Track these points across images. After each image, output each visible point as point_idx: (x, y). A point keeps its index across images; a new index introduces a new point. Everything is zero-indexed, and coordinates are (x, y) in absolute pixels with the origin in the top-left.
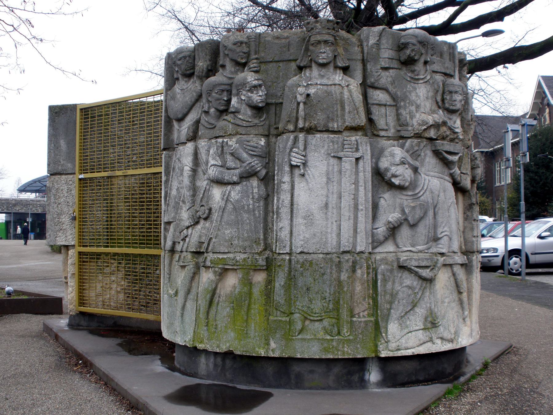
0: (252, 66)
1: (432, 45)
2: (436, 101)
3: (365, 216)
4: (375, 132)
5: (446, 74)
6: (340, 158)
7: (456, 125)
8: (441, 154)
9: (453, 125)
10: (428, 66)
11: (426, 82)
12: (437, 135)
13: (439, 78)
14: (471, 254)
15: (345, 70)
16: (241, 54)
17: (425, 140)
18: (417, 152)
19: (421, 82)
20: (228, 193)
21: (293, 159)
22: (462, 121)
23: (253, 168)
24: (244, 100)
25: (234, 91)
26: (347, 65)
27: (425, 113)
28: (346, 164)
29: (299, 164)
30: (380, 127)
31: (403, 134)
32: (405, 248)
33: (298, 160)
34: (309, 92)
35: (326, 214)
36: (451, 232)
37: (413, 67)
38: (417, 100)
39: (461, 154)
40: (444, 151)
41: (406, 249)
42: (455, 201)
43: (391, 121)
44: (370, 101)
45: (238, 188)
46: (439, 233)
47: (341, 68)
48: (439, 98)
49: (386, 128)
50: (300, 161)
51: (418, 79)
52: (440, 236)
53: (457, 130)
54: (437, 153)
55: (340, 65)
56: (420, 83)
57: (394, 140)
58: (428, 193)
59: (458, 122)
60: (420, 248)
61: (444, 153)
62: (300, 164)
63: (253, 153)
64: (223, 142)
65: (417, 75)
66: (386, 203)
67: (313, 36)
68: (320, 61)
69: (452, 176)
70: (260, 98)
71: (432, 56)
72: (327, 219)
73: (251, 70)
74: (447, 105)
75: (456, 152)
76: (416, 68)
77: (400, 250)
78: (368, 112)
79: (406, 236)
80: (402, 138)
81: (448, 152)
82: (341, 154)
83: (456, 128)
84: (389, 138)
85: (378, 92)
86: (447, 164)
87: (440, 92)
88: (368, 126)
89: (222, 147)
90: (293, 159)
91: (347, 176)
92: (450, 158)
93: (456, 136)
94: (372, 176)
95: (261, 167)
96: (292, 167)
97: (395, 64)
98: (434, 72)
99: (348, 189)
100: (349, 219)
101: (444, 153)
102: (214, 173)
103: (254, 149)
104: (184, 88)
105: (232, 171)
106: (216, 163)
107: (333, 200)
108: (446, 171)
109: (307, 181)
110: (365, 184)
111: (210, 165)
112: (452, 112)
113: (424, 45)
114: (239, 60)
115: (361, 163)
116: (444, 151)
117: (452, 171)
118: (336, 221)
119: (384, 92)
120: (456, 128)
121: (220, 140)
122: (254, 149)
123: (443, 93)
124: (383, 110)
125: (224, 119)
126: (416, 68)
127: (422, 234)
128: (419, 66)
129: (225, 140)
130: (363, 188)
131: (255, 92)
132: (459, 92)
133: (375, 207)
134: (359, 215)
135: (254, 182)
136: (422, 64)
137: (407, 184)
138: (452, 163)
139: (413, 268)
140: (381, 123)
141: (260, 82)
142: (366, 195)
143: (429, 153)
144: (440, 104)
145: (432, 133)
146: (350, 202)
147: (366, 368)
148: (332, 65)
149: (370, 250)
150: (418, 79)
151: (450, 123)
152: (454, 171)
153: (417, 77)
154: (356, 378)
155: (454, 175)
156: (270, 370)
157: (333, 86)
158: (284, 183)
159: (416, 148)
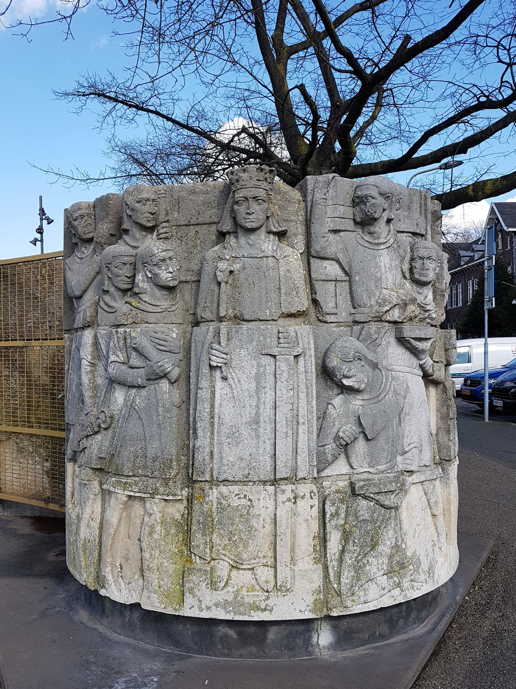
0: (161, 231)
1: (398, 195)
2: (402, 270)
3: (308, 431)
4: (321, 318)
5: (414, 234)
6: (274, 357)
7: (427, 300)
8: (408, 342)
9: (423, 302)
10: (391, 225)
11: (389, 247)
12: (403, 317)
13: (405, 239)
14: (447, 463)
15: (281, 235)
16: (148, 215)
17: (387, 324)
18: (377, 341)
19: (382, 247)
20: (132, 398)
21: (213, 358)
22: (434, 292)
23: (162, 368)
24: (151, 278)
25: (140, 266)
26: (283, 229)
27: (387, 289)
28: (282, 364)
29: (219, 365)
30: (328, 311)
31: (359, 318)
32: (361, 469)
33: (218, 360)
34: (232, 269)
35: (256, 430)
36: (421, 440)
37: (372, 229)
38: (377, 272)
39: (434, 339)
40: (413, 338)
41: (362, 470)
42: (426, 398)
43: (344, 301)
44: (313, 276)
45: (144, 392)
46: (406, 445)
47: (274, 233)
48: (406, 267)
49: (334, 311)
50: (221, 360)
51: (379, 244)
52: (407, 449)
53: (428, 308)
54: (402, 341)
55: (275, 230)
56: (242, 569)
57: (346, 326)
58: (390, 393)
59: (430, 296)
60: (382, 467)
61: (412, 341)
62: (221, 365)
63: (162, 348)
64: (125, 332)
65: (378, 238)
66: (335, 411)
67: (238, 191)
68: (247, 225)
69: (422, 367)
70: (171, 275)
71: (396, 210)
72: (258, 437)
73: (161, 236)
74: (417, 276)
75: (428, 337)
76: (377, 229)
77: (356, 471)
78: (313, 290)
79: (362, 454)
80: (356, 322)
81: (416, 339)
82: (275, 351)
83: (427, 305)
84: (338, 324)
85: (326, 263)
86: (415, 352)
87: (408, 258)
88: (312, 310)
89: (125, 339)
90: (213, 358)
91: (283, 380)
92: (420, 345)
93: (427, 314)
94: (317, 376)
95: (172, 367)
96: (211, 367)
97: (349, 225)
98: (399, 232)
99: (285, 397)
100: (286, 436)
101: (412, 341)
102: (114, 372)
103: (163, 343)
104: (84, 257)
105: (135, 370)
106: (117, 359)
107: (266, 412)
108: (415, 362)
109: (231, 387)
110: (307, 388)
111: (110, 361)
112: (422, 284)
113: (388, 197)
114: (145, 223)
115: (301, 360)
116: (413, 338)
117: (421, 362)
118: (269, 439)
119: (334, 262)
120: (427, 305)
121: (121, 330)
122: (163, 343)
123: (412, 259)
124: (331, 286)
125: (126, 302)
126: (377, 229)
127: (383, 450)
128: (381, 227)
129: (128, 330)
130: (304, 394)
131: (163, 268)
132: (433, 258)
133: (323, 417)
134: (300, 430)
135: (164, 384)
136: (384, 224)
137: (363, 386)
138: (423, 351)
139: (372, 495)
140: (328, 305)
141: (171, 254)
142: (309, 403)
143: (393, 341)
144: (407, 275)
145: (396, 315)
146: (287, 414)
147: (313, 628)
148: (263, 229)
149: (316, 475)
150: (379, 244)
151: (420, 299)
152: (424, 361)
153: (376, 241)
154: (300, 642)
155: (424, 366)
156: (189, 630)
157: (265, 259)
158: (202, 389)
159: (374, 337)
